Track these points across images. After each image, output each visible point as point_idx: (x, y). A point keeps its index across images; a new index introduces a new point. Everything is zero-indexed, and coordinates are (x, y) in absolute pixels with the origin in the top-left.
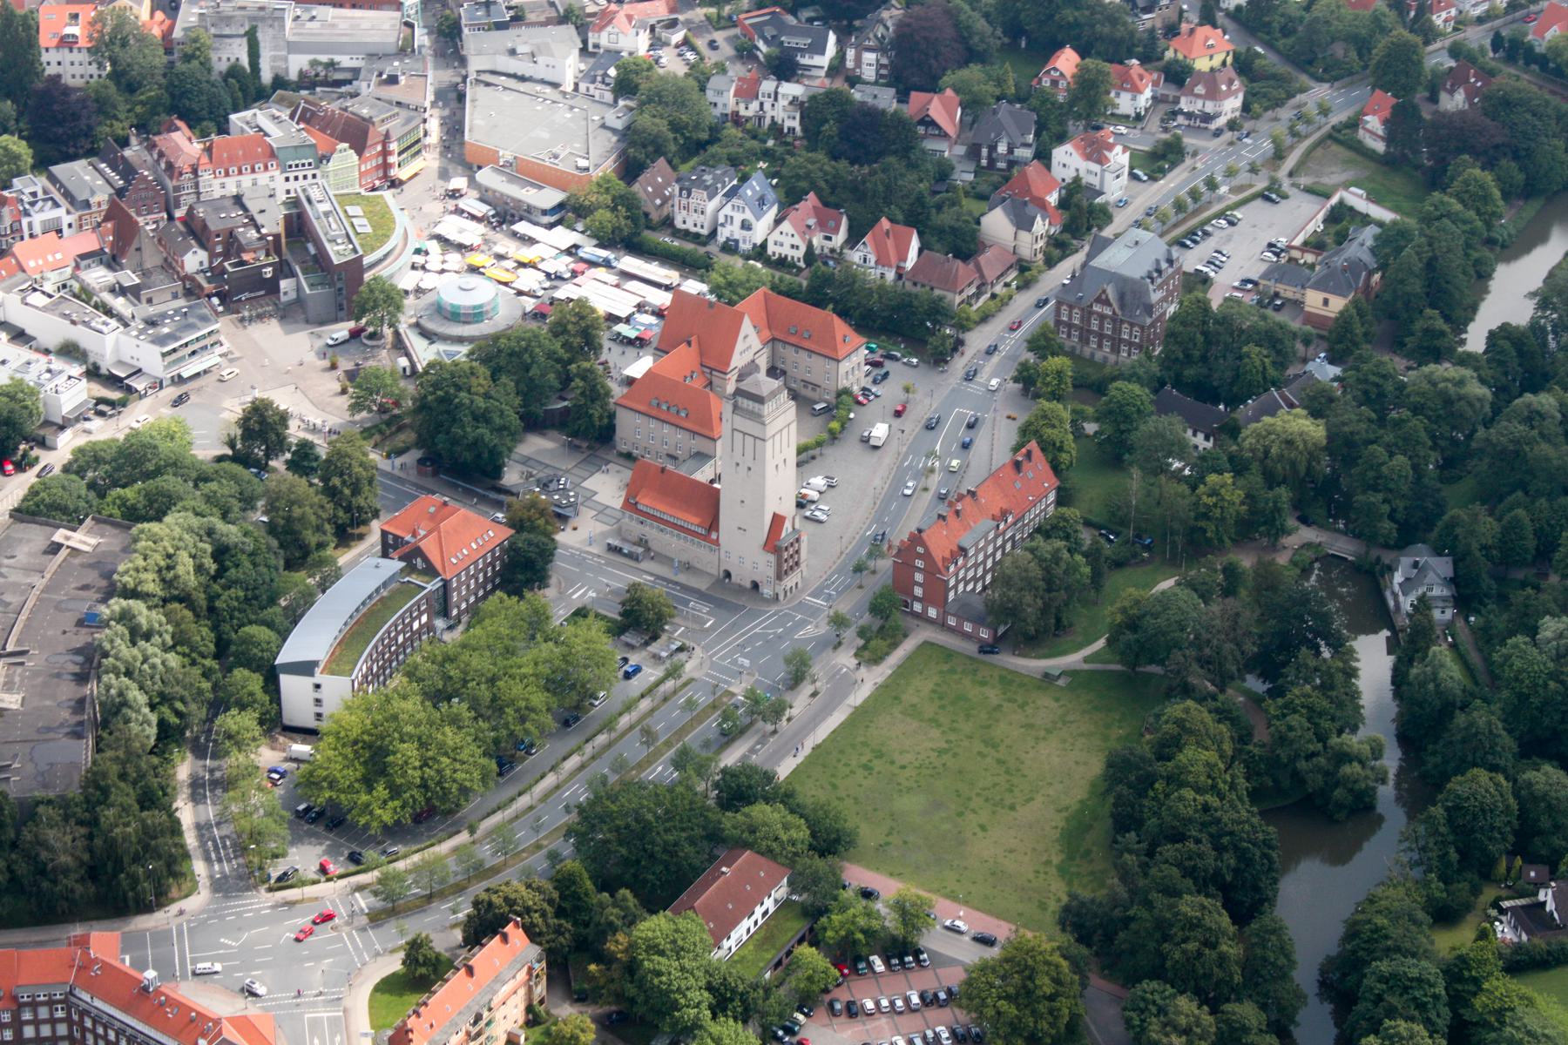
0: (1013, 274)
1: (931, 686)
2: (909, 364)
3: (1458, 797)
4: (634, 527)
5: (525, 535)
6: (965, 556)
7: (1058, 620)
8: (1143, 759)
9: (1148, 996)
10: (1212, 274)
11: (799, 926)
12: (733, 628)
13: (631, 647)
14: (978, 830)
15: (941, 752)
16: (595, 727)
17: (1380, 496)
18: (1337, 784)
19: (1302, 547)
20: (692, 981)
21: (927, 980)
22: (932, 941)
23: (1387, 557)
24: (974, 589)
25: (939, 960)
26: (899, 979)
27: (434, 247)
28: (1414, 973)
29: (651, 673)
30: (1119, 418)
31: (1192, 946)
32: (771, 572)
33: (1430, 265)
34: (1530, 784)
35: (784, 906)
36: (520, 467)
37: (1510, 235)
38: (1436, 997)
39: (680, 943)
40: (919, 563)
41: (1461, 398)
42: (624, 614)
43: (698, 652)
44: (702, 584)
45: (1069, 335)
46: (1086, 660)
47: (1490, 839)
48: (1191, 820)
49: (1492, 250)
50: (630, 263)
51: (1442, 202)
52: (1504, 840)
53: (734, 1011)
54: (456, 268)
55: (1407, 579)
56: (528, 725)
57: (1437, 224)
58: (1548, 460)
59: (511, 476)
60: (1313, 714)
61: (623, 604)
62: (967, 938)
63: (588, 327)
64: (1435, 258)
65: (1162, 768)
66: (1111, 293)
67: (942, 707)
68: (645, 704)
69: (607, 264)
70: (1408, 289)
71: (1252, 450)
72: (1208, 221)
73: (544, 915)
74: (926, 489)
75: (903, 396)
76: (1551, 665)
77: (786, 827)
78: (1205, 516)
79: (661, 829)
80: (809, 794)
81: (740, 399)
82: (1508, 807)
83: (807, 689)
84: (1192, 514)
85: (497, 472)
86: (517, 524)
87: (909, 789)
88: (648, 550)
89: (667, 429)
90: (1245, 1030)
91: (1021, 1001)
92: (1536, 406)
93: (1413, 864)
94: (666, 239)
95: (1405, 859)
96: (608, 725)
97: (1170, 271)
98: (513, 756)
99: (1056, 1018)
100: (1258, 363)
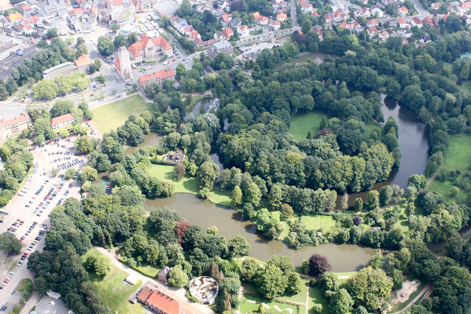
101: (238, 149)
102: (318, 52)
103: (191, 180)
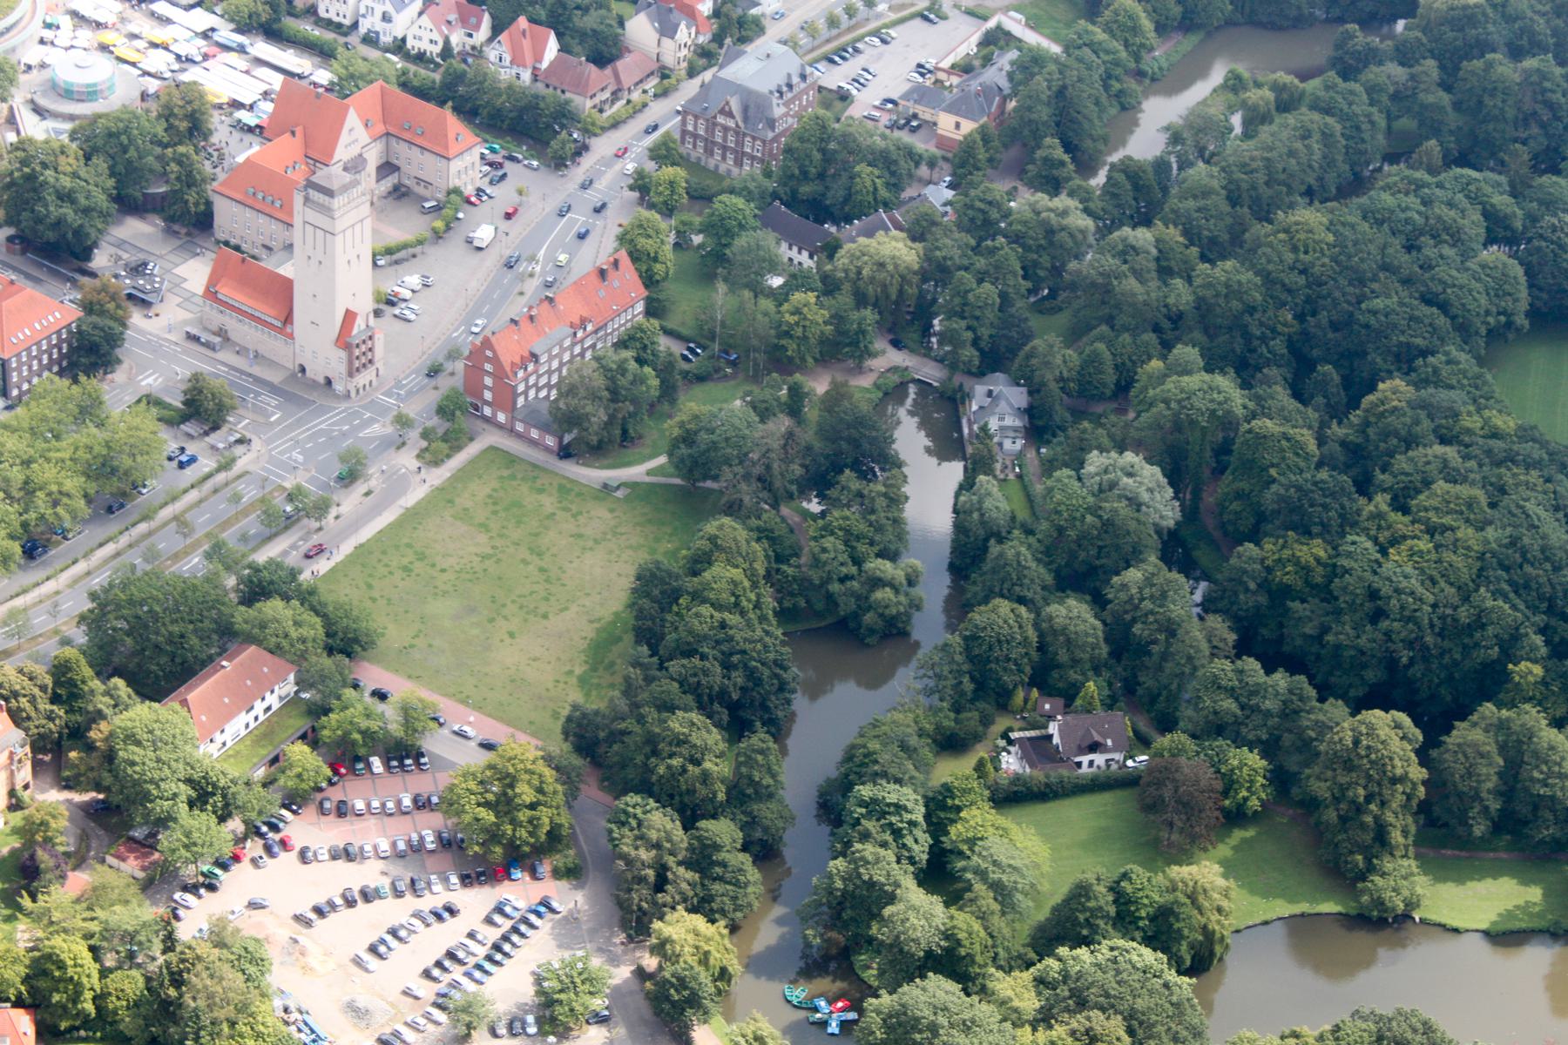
0: (654, 81)
1: (487, 490)
2: (528, 167)
3: (976, 626)
4: (217, 318)
5: (94, 319)
6: (537, 361)
7: (625, 432)
8: (670, 574)
9: (630, 809)
10: (854, 92)
11: (301, 724)
12: (299, 423)
13: (190, 436)
14: (506, 637)
15: (484, 557)
16: (135, 517)
17: (963, 324)
18: (870, 608)
19: (888, 370)
20: (167, 771)
21: (427, 784)
22: (436, 744)
23: (968, 382)
24: (547, 397)
25: (441, 764)
26: (397, 780)
27: (66, 22)
28: (892, 798)
29: (206, 464)
30: (721, 230)
31: (676, 762)
32: (343, 368)
33: (1061, 93)
34: (1051, 618)
35: (291, 703)
36: (113, 250)
37: (1160, 68)
38: (912, 824)
39: (158, 733)
40: (488, 367)
41: (1063, 229)
42: (186, 403)
43: (257, 444)
44: (275, 377)
45: (695, 146)
46: (649, 473)
47: (1005, 669)
48: (705, 637)
49: (1140, 83)
50: (263, 48)
51: (1087, 32)
52: (1020, 671)
53: (214, 806)
54: (86, 45)
55: (981, 408)
56: (59, 510)
57: (1077, 52)
58: (1134, 295)
59: (101, 260)
60: (850, 538)
61: (185, 393)
62: (473, 744)
63: (194, 111)
64: (1064, 87)
65: (691, 583)
66: (735, 105)
67: (495, 513)
68: (193, 495)
69: (241, 50)
70: (1034, 116)
71: (846, 271)
72: (860, 39)
73: (33, 700)
74: (521, 293)
75: (516, 199)
76: (1091, 499)
77: (297, 624)
78: (787, 334)
79: (167, 620)
80: (332, 596)
81: (311, 191)
82: (1026, 639)
83: (360, 488)
84: (773, 332)
85: (86, 253)
86: (88, 307)
87: (445, 593)
88: (227, 339)
89: (262, 219)
90: (717, 847)
91: (500, 808)
92: (1131, 240)
93: (928, 692)
94: (307, 28)
95: (919, 686)
96: (145, 518)
97: (803, 86)
98: (48, 540)
99: (536, 827)
100: (868, 184)
101: (1434, 606)
102: (1230, 23)
103: (1244, 841)
